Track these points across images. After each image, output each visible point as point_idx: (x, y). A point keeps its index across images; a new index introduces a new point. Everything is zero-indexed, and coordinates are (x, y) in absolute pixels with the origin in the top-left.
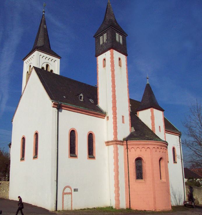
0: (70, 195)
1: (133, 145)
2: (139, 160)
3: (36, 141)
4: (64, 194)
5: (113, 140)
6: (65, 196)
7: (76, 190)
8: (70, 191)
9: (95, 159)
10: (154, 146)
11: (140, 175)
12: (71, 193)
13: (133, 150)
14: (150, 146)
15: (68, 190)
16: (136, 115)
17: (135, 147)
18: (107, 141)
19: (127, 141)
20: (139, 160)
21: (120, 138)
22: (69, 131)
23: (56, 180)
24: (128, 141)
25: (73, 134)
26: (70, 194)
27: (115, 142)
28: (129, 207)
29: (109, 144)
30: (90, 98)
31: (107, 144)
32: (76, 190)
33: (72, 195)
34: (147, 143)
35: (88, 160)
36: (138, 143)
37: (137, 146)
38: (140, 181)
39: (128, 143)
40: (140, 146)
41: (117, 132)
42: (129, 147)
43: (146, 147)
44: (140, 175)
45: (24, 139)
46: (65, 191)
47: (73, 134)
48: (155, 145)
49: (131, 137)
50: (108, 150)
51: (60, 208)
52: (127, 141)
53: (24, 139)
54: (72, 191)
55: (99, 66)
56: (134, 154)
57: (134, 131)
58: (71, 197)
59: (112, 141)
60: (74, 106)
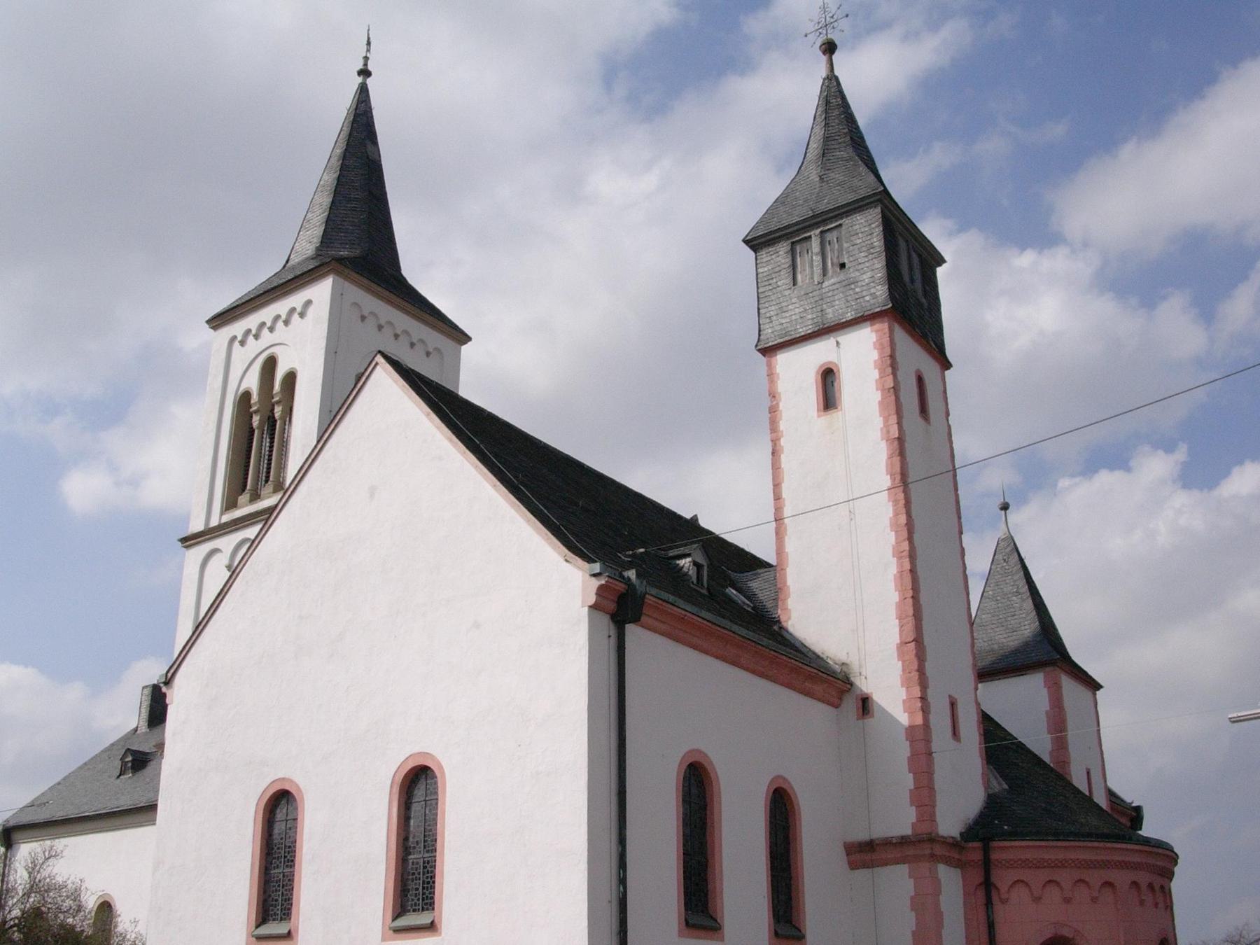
3: (435, 820)
13: (1019, 896)
16: (255, 398)
18: (863, 836)
21: (950, 823)
22: (681, 763)
25: (697, 785)
37: (1044, 875)
39: (995, 856)
41: (936, 787)
42: (1003, 878)
43: (1096, 877)
45: (279, 807)
47: (697, 785)
50: (989, 903)
52: (986, 841)
53: (279, 807)
55: (892, 537)
57: (1006, 786)
59: (903, 841)
60: (704, 614)
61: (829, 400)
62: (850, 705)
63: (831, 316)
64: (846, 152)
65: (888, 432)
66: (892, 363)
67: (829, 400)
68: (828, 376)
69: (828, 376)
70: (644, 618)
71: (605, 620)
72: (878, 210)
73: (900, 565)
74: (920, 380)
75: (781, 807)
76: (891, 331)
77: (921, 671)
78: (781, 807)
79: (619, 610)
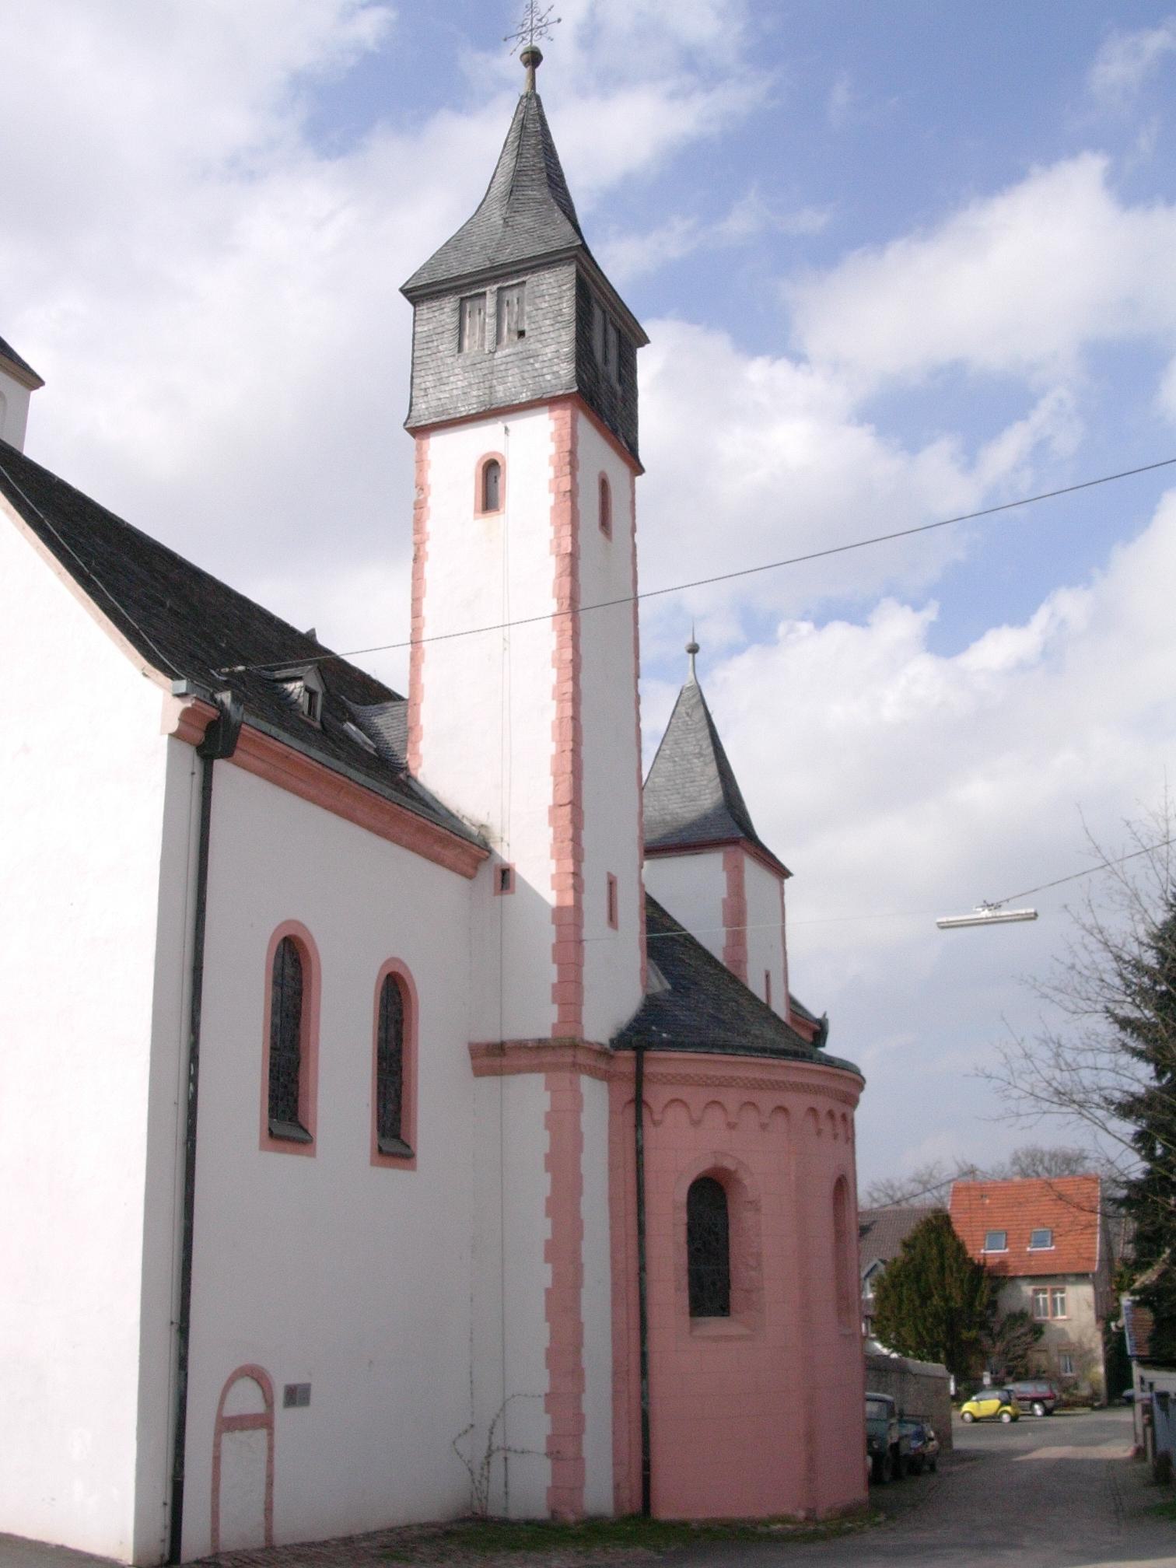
0: (262, 1434)
1: (685, 1080)
2: (711, 1196)
4: (228, 1424)
5: (546, 1033)
6: (226, 1438)
7: (297, 1396)
8: (259, 1408)
9: (413, 1168)
10: (809, 1100)
11: (711, 1289)
12: (264, 1421)
13: (676, 1117)
14: (790, 1100)
15: (247, 1399)
17: (697, 1097)
18: (492, 1036)
19: (640, 1050)
20: (711, 1196)
23: (176, 1318)
24: (647, 1054)
25: (292, 963)
26: (261, 1426)
27: (570, 1052)
28: (638, 1505)
29: (505, 1061)
30: (343, 721)
31: (486, 1061)
32: (297, 1396)
33: (271, 1435)
34: (779, 1076)
35: (375, 1169)
36: (719, 1074)
38: (714, 1325)
39: (649, 1069)
40: (732, 1098)
42: (657, 1096)
43: (767, 1100)
44: (711, 1289)
46: (232, 1409)
47: (292, 963)
48: (817, 1090)
49: (640, 1037)
51: (195, 1542)
52: (640, 1050)
54: (269, 1403)
56: (681, 1152)
57: (669, 987)
58: (264, 1444)
59: (541, 1045)
61: (489, 501)
62: (487, 877)
63: (502, 395)
64: (539, 192)
65: (559, 545)
66: (572, 460)
67: (489, 501)
68: (491, 469)
69: (491, 469)
70: (237, 753)
71: (189, 754)
72: (572, 269)
73: (560, 710)
74: (604, 485)
75: (395, 997)
76: (574, 420)
77: (576, 840)
78: (395, 997)
79: (208, 741)
